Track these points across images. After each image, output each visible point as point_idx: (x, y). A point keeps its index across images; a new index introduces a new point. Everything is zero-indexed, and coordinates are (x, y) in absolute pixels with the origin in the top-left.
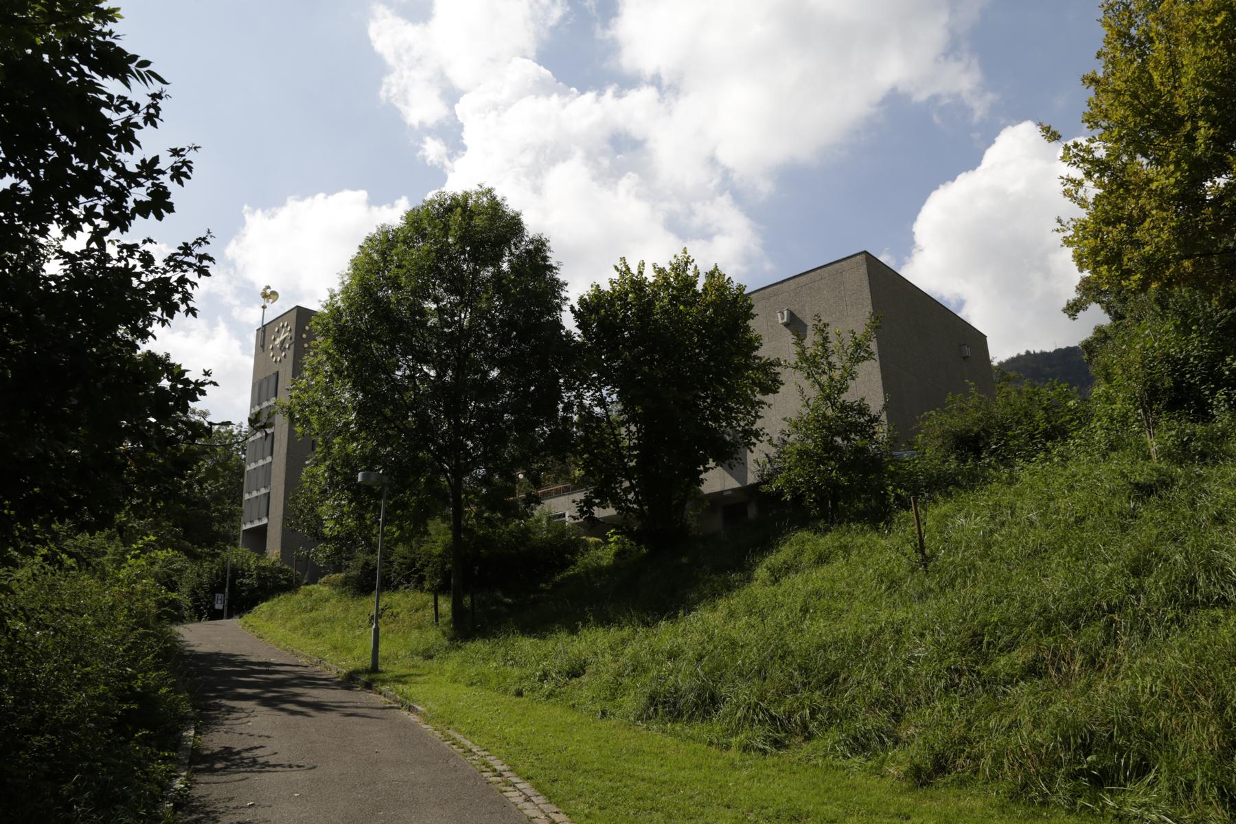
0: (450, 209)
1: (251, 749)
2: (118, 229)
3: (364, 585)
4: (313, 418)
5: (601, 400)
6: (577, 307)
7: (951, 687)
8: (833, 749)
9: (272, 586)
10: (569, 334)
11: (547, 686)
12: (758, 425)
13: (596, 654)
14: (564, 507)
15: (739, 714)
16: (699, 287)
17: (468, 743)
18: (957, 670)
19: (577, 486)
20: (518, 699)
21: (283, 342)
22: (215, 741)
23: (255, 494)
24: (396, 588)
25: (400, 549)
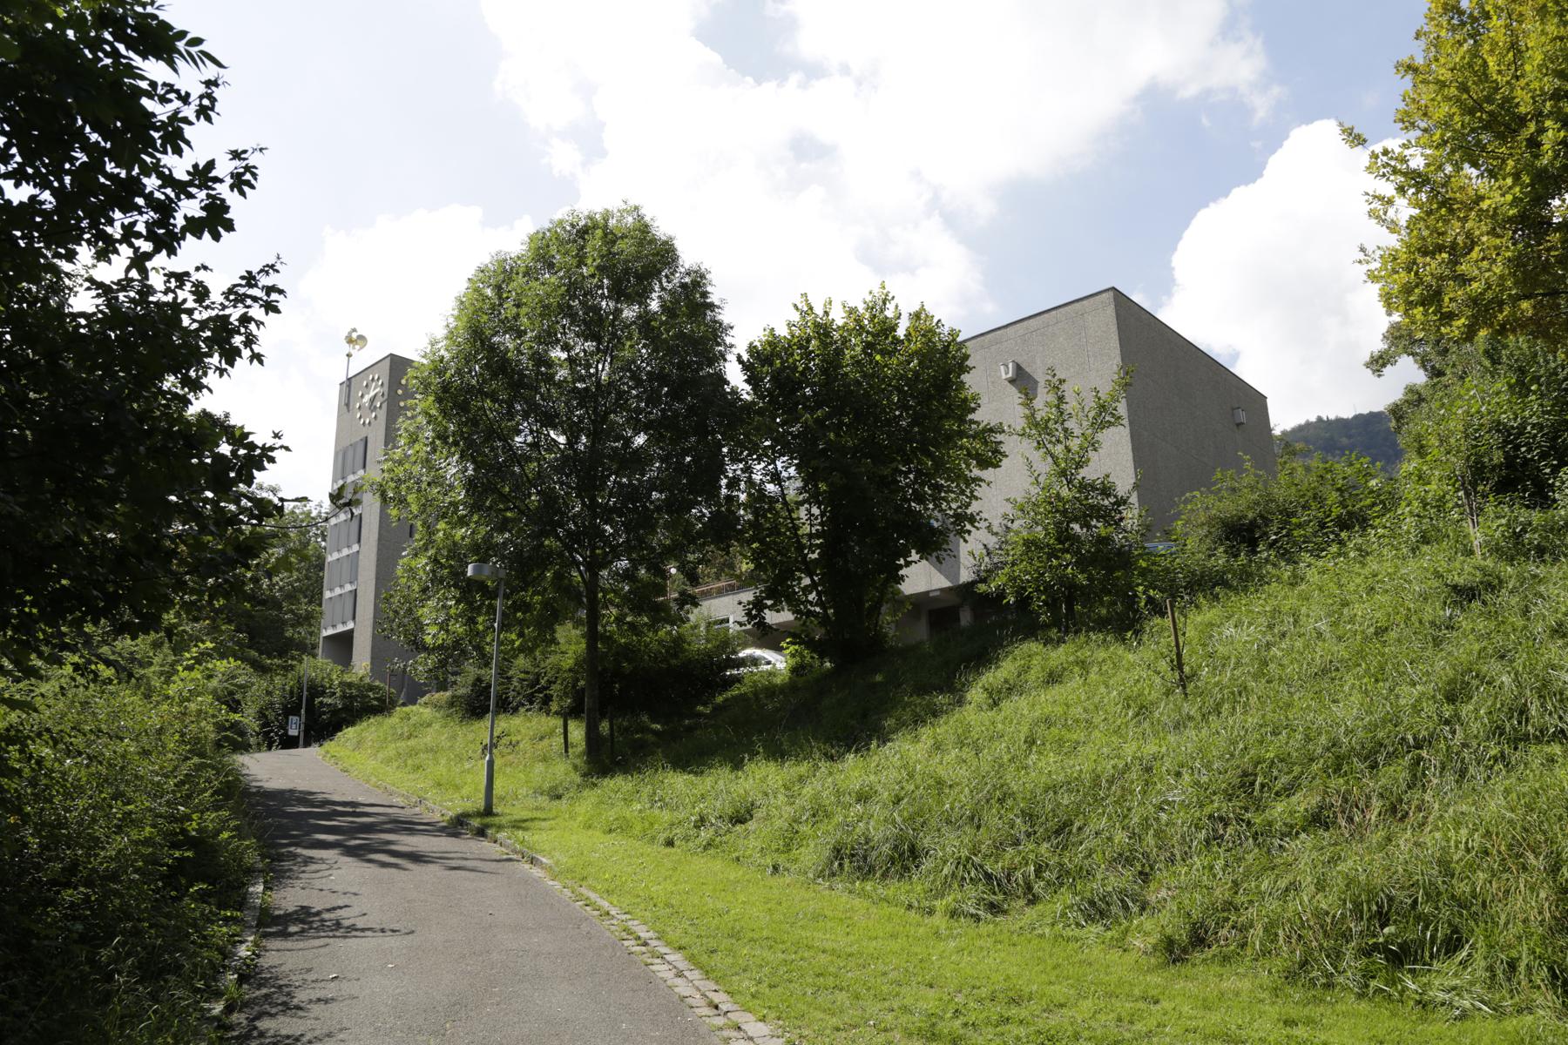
0: (584, 232)
1: (334, 909)
2: (164, 252)
3: (476, 706)
4: (410, 498)
5: (776, 476)
6: (745, 357)
8: (1063, 915)
9: (360, 706)
10: (734, 391)
11: (705, 835)
12: (974, 507)
15: (945, 871)
17: (605, 904)
19: (744, 583)
20: (669, 850)
21: (372, 400)
22: (288, 898)
23: (338, 591)
25: (521, 661)
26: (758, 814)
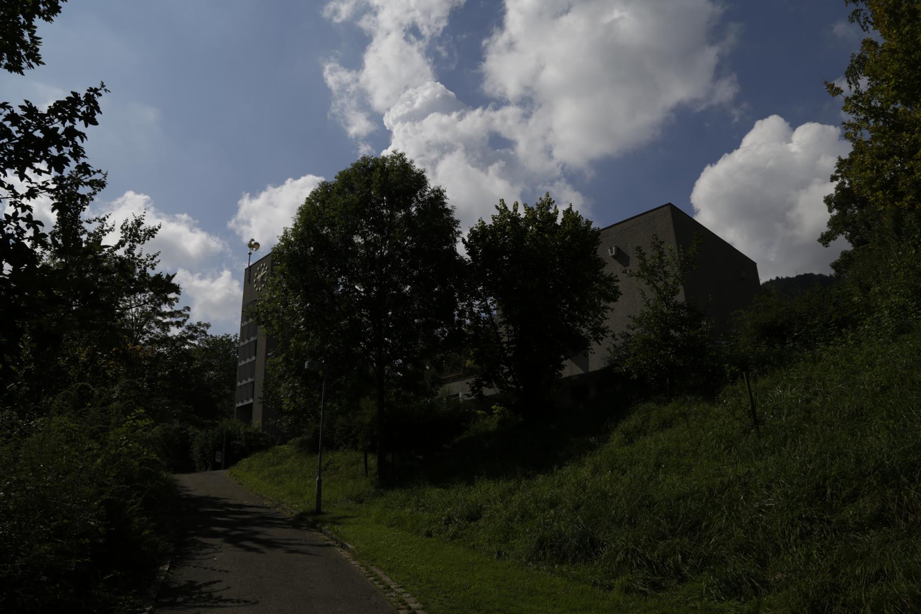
0: (372, 169)
1: (211, 583)
3: (312, 447)
4: (274, 322)
5: (484, 307)
6: (467, 240)
7: (805, 535)
8: (707, 591)
9: (256, 445)
10: (461, 259)
11: (451, 529)
12: (605, 324)
13: (489, 501)
14: (460, 389)
15: (618, 559)
16: (559, 221)
17: (388, 579)
18: (807, 519)
19: (469, 372)
20: (428, 539)
21: (262, 277)
22: (186, 574)
23: (244, 382)
24: (337, 448)
25: (341, 420)
26: (486, 515)
